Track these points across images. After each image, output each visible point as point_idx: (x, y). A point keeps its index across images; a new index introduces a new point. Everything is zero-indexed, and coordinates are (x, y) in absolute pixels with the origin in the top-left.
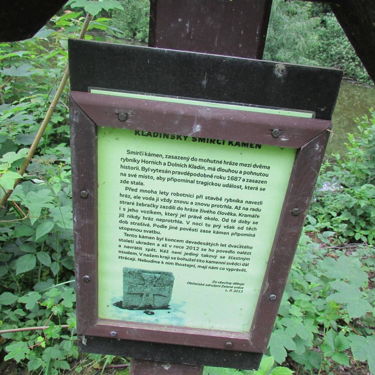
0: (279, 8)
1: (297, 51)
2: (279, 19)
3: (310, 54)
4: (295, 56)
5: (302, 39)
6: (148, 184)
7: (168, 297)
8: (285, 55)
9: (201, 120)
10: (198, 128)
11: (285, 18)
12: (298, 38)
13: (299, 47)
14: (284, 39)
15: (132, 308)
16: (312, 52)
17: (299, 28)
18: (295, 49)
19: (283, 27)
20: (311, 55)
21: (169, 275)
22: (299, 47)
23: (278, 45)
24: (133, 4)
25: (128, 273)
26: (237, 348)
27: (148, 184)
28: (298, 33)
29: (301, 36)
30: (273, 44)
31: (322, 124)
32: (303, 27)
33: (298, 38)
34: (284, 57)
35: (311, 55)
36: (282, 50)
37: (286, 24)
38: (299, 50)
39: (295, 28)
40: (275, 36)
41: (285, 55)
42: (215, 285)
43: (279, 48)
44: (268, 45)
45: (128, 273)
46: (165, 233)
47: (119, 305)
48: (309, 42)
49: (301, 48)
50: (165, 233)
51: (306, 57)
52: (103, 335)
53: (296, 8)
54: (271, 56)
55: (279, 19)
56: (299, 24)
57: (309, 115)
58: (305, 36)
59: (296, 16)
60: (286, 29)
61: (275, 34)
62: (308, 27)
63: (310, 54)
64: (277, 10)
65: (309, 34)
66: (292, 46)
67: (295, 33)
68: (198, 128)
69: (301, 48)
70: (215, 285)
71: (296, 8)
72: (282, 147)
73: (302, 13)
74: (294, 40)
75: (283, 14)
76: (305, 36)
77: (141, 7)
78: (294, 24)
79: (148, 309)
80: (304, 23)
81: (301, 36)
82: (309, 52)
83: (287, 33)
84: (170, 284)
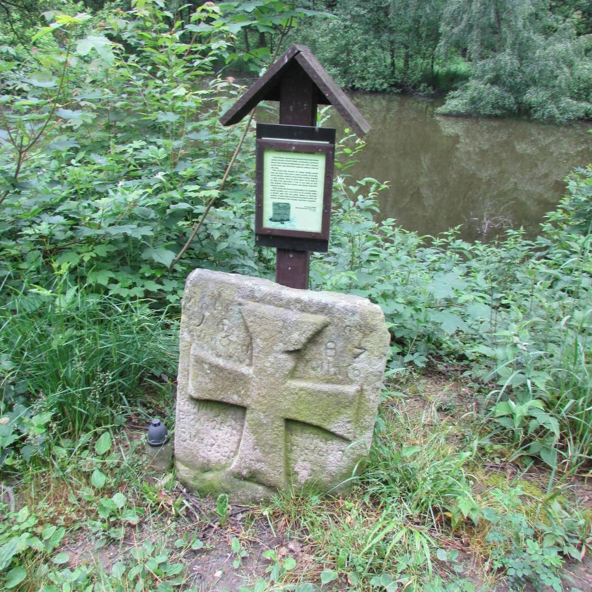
0: (528, 24)
1: (557, 89)
2: (528, 41)
3: (581, 92)
4: (554, 98)
5: (566, 69)
6: (281, 168)
7: (288, 215)
8: (536, 97)
9: (295, 145)
10: (294, 148)
11: (538, 39)
12: (559, 68)
13: (560, 82)
14: (536, 71)
15: (276, 221)
16: (585, 88)
17: (559, 53)
18: (554, 87)
19: (534, 53)
20: (581, 94)
21: (288, 204)
22: (560, 82)
23: (526, 81)
24: (303, 33)
25: (275, 204)
26: (317, 238)
27: (281, 168)
28: (558, 61)
29: (563, 66)
30: (518, 80)
31: (332, 145)
32: (567, 50)
33: (559, 68)
34: (535, 99)
35: (581, 94)
36: (532, 90)
37: (539, 47)
38: (560, 86)
39: (553, 53)
40: (522, 68)
41: (536, 97)
42: (306, 208)
43: (528, 86)
44: (510, 82)
45: (275, 204)
46: (287, 186)
47: (271, 220)
48: (577, 74)
49: (563, 85)
50: (287, 186)
51: (572, 97)
52: (264, 233)
53: (557, 21)
54: (516, 98)
55: (528, 41)
56: (560, 47)
57: (328, 143)
58: (570, 65)
59: (556, 34)
60: (539, 57)
61: (521, 64)
62: (574, 51)
63: (581, 92)
64: (524, 27)
65: (577, 62)
66: (549, 82)
67: (554, 61)
68: (294, 148)
69: (563, 85)
70: (306, 208)
71: (557, 21)
72: (321, 153)
73: (565, 29)
74: (552, 72)
75: (534, 33)
76: (570, 65)
77: (315, 36)
78: (551, 48)
79: (282, 221)
80: (569, 45)
81: (563, 66)
82: (579, 90)
83: (541, 63)
84: (289, 208)
